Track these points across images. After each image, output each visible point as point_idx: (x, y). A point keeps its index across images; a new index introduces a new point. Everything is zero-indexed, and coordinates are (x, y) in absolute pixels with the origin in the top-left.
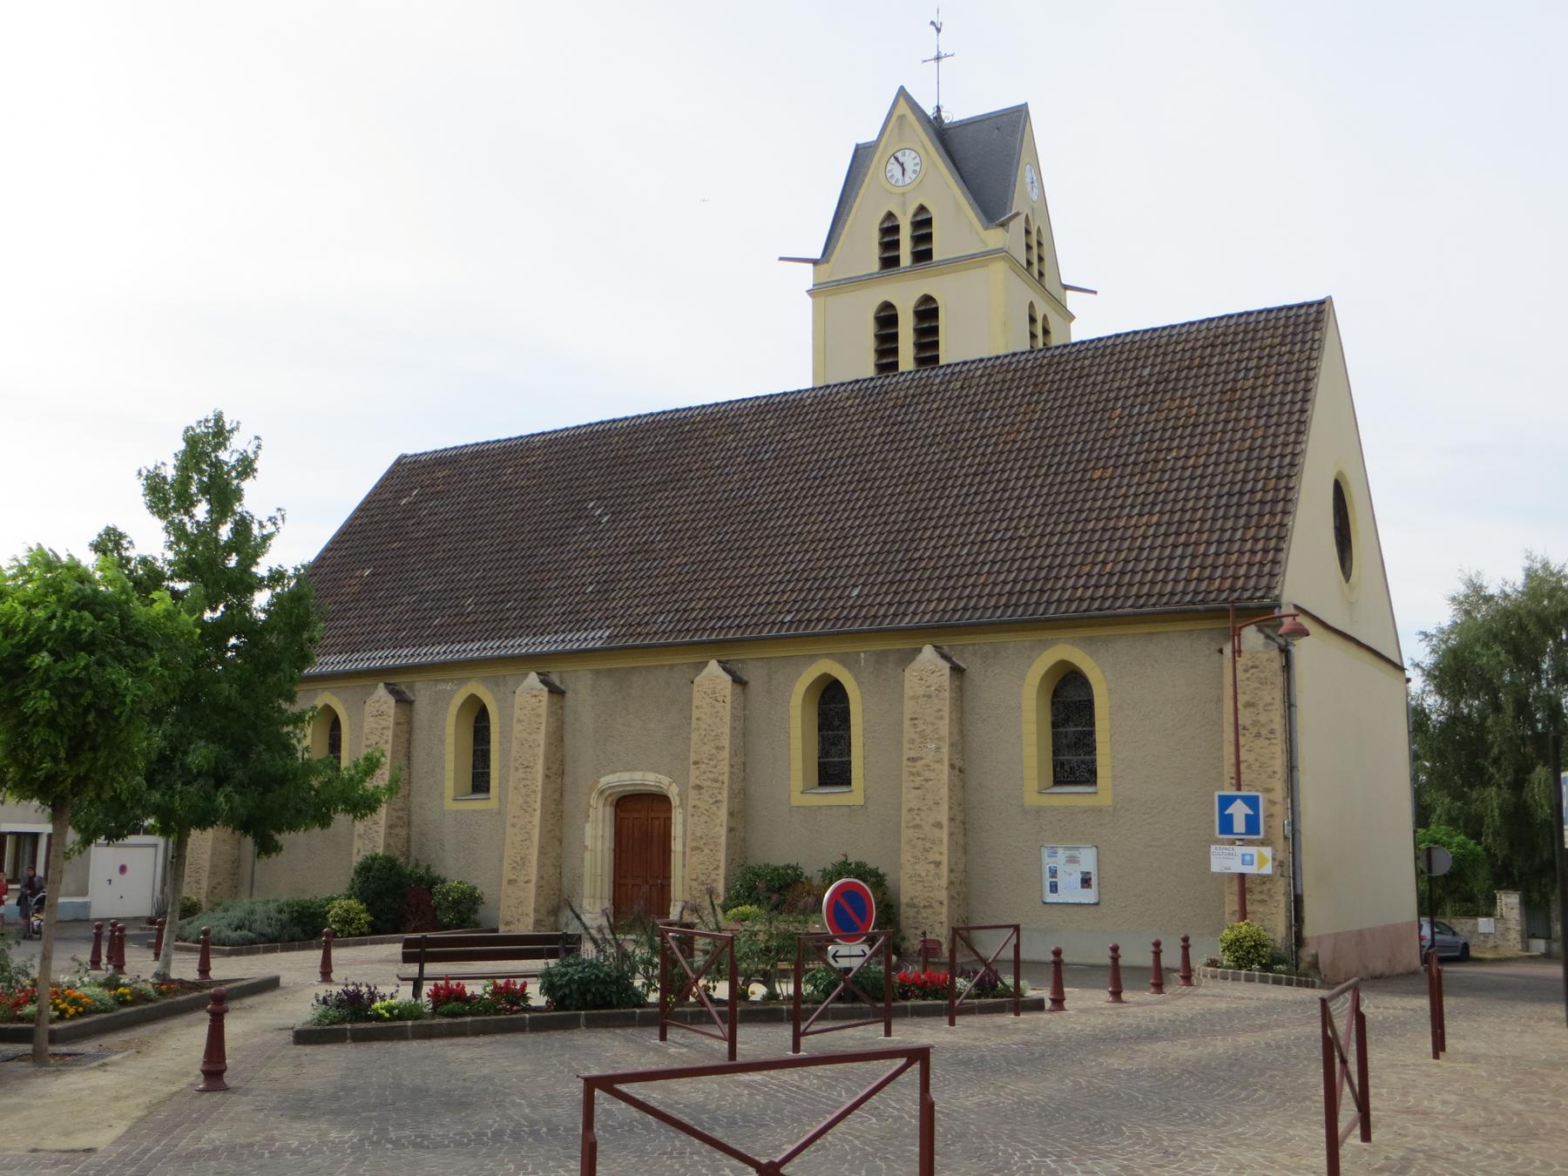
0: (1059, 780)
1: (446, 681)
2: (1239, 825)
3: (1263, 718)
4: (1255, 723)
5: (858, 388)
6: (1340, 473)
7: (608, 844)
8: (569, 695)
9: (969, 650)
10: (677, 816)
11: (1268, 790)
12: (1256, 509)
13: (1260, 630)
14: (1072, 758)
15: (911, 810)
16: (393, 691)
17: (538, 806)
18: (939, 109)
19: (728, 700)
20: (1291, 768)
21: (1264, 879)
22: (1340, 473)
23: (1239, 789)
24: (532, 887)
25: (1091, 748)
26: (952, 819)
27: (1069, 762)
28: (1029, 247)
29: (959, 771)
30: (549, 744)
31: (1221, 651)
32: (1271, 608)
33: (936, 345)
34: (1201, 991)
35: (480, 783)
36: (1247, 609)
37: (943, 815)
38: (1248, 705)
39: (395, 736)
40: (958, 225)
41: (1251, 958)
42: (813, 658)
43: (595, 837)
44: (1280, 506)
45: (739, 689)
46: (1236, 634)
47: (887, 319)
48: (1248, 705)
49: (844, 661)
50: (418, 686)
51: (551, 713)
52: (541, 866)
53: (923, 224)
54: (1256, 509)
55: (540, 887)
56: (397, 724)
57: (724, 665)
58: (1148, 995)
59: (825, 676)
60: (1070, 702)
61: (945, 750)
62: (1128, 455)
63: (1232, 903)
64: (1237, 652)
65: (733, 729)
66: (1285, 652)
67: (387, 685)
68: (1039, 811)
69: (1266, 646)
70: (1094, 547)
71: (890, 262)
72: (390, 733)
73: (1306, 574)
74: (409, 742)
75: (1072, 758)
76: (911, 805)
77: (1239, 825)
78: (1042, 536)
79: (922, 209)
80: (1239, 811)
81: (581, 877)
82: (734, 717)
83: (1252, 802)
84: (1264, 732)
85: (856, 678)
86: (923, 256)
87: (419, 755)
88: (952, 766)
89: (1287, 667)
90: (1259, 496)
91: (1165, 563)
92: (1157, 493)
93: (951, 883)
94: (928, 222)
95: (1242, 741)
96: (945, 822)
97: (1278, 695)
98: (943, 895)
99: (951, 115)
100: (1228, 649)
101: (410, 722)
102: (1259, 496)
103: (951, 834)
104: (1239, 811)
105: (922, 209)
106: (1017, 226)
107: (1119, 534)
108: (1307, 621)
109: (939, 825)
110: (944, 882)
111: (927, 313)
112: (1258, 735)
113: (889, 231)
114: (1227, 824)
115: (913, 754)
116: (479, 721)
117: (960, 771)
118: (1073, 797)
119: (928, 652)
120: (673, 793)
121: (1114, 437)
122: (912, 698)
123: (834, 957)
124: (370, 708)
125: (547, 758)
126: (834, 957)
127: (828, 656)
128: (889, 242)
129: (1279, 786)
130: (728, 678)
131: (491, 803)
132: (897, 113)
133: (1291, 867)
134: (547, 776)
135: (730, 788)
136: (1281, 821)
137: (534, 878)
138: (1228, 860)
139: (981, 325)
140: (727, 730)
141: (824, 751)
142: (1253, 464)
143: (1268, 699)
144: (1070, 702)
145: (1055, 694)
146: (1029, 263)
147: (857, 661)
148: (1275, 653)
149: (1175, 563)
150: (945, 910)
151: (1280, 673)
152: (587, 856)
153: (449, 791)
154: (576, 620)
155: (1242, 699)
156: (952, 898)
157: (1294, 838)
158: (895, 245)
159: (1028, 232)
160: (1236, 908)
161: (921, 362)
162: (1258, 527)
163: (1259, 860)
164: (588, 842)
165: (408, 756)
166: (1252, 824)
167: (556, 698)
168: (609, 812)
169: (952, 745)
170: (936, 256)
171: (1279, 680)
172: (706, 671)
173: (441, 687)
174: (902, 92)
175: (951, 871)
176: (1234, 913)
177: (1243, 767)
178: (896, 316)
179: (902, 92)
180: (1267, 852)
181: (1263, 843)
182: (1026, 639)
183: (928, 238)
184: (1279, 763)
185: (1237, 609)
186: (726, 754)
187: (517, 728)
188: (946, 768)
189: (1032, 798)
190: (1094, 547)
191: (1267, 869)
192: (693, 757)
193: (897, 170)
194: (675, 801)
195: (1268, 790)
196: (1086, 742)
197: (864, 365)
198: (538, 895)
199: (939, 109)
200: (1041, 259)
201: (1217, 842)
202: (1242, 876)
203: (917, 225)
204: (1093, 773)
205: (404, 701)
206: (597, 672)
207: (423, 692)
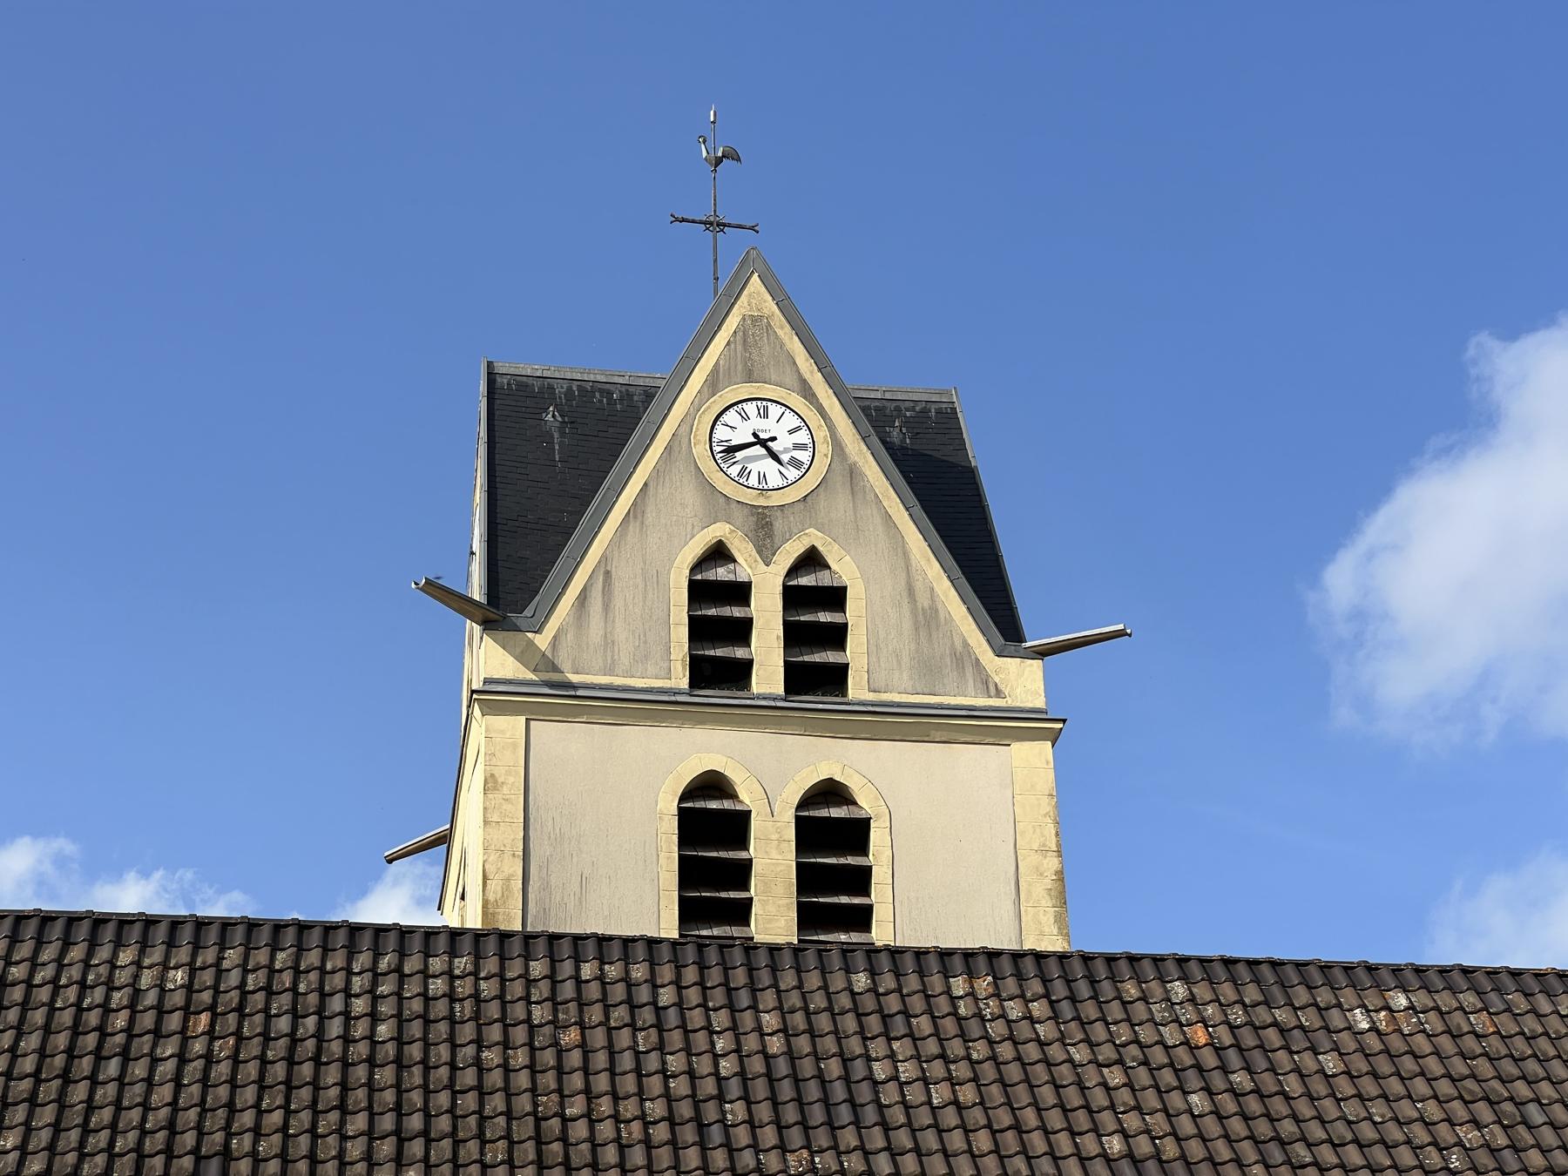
40: (891, 574)
47: (710, 827)
53: (815, 609)
71: (717, 670)
79: (811, 560)
94: (835, 597)
99: (501, 368)
105: (811, 560)
111: (833, 836)
113: (716, 606)
158: (741, 631)
161: (809, 917)
170: (857, 689)
183: (836, 636)
203: (793, 597)
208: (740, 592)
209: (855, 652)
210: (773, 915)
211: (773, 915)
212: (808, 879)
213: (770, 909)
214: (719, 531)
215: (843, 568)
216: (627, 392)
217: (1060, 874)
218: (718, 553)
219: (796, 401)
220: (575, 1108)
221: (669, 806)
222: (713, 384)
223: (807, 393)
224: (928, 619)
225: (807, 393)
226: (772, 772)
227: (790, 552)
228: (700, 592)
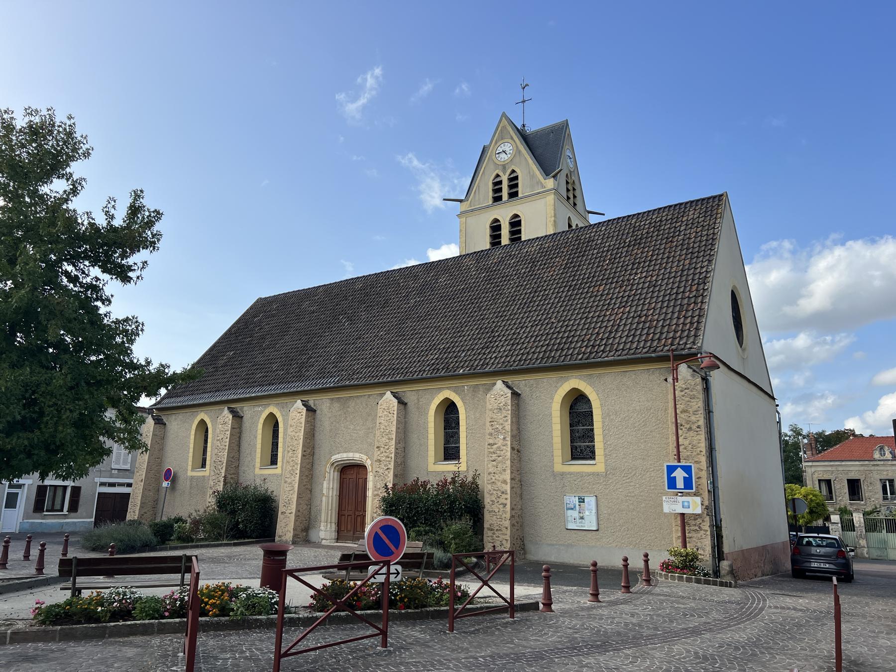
0: (574, 458)
1: (259, 406)
2: (680, 484)
3: (693, 418)
4: (688, 422)
5: (479, 255)
6: (734, 287)
7: (336, 493)
8: (318, 412)
9: (522, 382)
10: (370, 477)
11: (696, 462)
12: (686, 301)
13: (689, 367)
14: (581, 445)
15: (490, 474)
16: (232, 411)
17: (298, 472)
18: (524, 126)
19: (395, 412)
20: (711, 449)
21: (696, 516)
22: (734, 287)
23: (679, 462)
24: (293, 516)
25: (592, 439)
26: (512, 479)
27: (580, 446)
28: (568, 190)
29: (518, 451)
30: (305, 438)
31: (666, 380)
32: (696, 354)
33: (519, 232)
34: (657, 590)
35: (274, 462)
36: (682, 355)
37: (507, 476)
38: (684, 411)
39: (231, 435)
40: (528, 169)
41: (685, 565)
42: (440, 389)
43: (328, 488)
44: (700, 299)
45: (402, 407)
46: (675, 369)
47: (496, 227)
48: (684, 411)
49: (456, 390)
50: (245, 408)
51: (307, 422)
52: (298, 504)
53: (514, 181)
54: (686, 301)
55: (297, 516)
56: (233, 428)
57: (395, 395)
58: (619, 595)
59: (447, 399)
60: (578, 410)
61: (509, 439)
62: (613, 278)
63: (677, 533)
64: (676, 379)
65: (398, 428)
66: (705, 380)
67: (229, 408)
68: (563, 474)
69: (693, 376)
70: (593, 325)
71: (497, 199)
72: (229, 433)
73: (715, 335)
74: (240, 438)
75: (581, 445)
76: (490, 470)
77: (680, 484)
78: (564, 321)
79: (513, 171)
80: (679, 475)
81: (320, 510)
82: (398, 422)
83: (687, 469)
84: (694, 427)
85: (462, 399)
86: (513, 195)
87: (244, 445)
88: (513, 449)
89: (707, 389)
90: (687, 294)
91: (632, 332)
92: (629, 296)
93: (512, 516)
94: (516, 178)
95: (680, 432)
96: (509, 481)
97: (701, 404)
98: (507, 523)
99: (532, 127)
100: (670, 380)
101: (240, 427)
102: (687, 294)
103: (512, 488)
104: (679, 475)
105: (513, 171)
106: (562, 178)
107: (607, 318)
108: (717, 363)
109: (505, 482)
110: (508, 516)
111: (516, 223)
112: (690, 429)
113: (497, 184)
114: (672, 483)
115: (491, 441)
116: (273, 424)
117: (518, 451)
118: (581, 467)
119: (499, 384)
120: (368, 464)
121: (606, 270)
122: (491, 410)
123: (398, 573)
124: (220, 420)
125: (303, 446)
126: (398, 573)
127: (448, 388)
128: (497, 190)
129: (703, 460)
130: (396, 401)
131: (277, 470)
132: (501, 125)
133: (713, 509)
134: (303, 456)
135: (395, 462)
136: (705, 483)
137: (294, 511)
138: (674, 505)
139: (540, 216)
140: (394, 429)
141: (447, 441)
142: (684, 278)
143: (695, 408)
144: (578, 410)
145: (571, 408)
146: (568, 198)
147: (464, 391)
148: (699, 380)
149: (638, 332)
150: (508, 532)
151: (701, 392)
152: (324, 499)
153: (258, 465)
154: (322, 373)
155: (680, 407)
156: (513, 525)
157: (714, 492)
158: (500, 190)
159: (567, 183)
160: (680, 534)
161: (512, 240)
162: (687, 311)
163: (694, 505)
164: (324, 492)
165: (239, 446)
166: (688, 483)
167: (310, 414)
168: (337, 475)
169: (512, 436)
170: (520, 195)
171: (701, 396)
172: (384, 397)
173: (256, 409)
174: (504, 115)
175: (512, 509)
176: (678, 538)
177: (681, 448)
178: (500, 225)
179: (504, 115)
180: (698, 500)
181: (695, 495)
182: (553, 376)
183: (516, 185)
184: (703, 446)
185: (674, 356)
186: (393, 442)
187: (290, 430)
188: (509, 449)
189: (559, 467)
190: (593, 325)
191: (698, 510)
192: (377, 444)
193: (503, 155)
194: (369, 468)
195: (696, 462)
196: (589, 435)
197: (484, 243)
198: (296, 521)
199: (524, 126)
200: (575, 197)
201: (666, 494)
202: (683, 515)
203: (510, 180)
204: (593, 452)
205: (237, 416)
206: (332, 399)
207: (247, 410)
208: (500, 182)
209: (520, 189)
210: (505, 240)
211: (505, 240)
212: (512, 233)
213: (507, 238)
214: (497, 172)
215: (519, 172)
216: (563, 123)
217: (555, 221)
218: (498, 176)
219: (510, 141)
220: (585, 267)
221: (488, 227)
222: (496, 143)
223: (512, 138)
224: (533, 176)
225: (512, 138)
226: (504, 214)
227: (509, 171)
228: (495, 184)
